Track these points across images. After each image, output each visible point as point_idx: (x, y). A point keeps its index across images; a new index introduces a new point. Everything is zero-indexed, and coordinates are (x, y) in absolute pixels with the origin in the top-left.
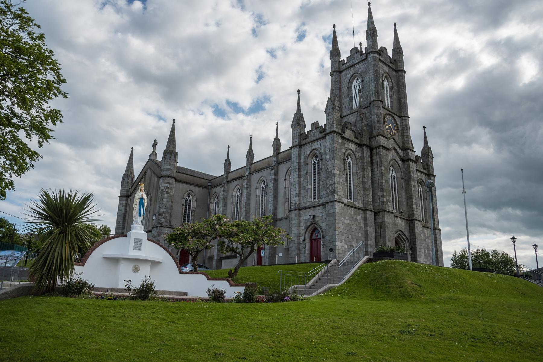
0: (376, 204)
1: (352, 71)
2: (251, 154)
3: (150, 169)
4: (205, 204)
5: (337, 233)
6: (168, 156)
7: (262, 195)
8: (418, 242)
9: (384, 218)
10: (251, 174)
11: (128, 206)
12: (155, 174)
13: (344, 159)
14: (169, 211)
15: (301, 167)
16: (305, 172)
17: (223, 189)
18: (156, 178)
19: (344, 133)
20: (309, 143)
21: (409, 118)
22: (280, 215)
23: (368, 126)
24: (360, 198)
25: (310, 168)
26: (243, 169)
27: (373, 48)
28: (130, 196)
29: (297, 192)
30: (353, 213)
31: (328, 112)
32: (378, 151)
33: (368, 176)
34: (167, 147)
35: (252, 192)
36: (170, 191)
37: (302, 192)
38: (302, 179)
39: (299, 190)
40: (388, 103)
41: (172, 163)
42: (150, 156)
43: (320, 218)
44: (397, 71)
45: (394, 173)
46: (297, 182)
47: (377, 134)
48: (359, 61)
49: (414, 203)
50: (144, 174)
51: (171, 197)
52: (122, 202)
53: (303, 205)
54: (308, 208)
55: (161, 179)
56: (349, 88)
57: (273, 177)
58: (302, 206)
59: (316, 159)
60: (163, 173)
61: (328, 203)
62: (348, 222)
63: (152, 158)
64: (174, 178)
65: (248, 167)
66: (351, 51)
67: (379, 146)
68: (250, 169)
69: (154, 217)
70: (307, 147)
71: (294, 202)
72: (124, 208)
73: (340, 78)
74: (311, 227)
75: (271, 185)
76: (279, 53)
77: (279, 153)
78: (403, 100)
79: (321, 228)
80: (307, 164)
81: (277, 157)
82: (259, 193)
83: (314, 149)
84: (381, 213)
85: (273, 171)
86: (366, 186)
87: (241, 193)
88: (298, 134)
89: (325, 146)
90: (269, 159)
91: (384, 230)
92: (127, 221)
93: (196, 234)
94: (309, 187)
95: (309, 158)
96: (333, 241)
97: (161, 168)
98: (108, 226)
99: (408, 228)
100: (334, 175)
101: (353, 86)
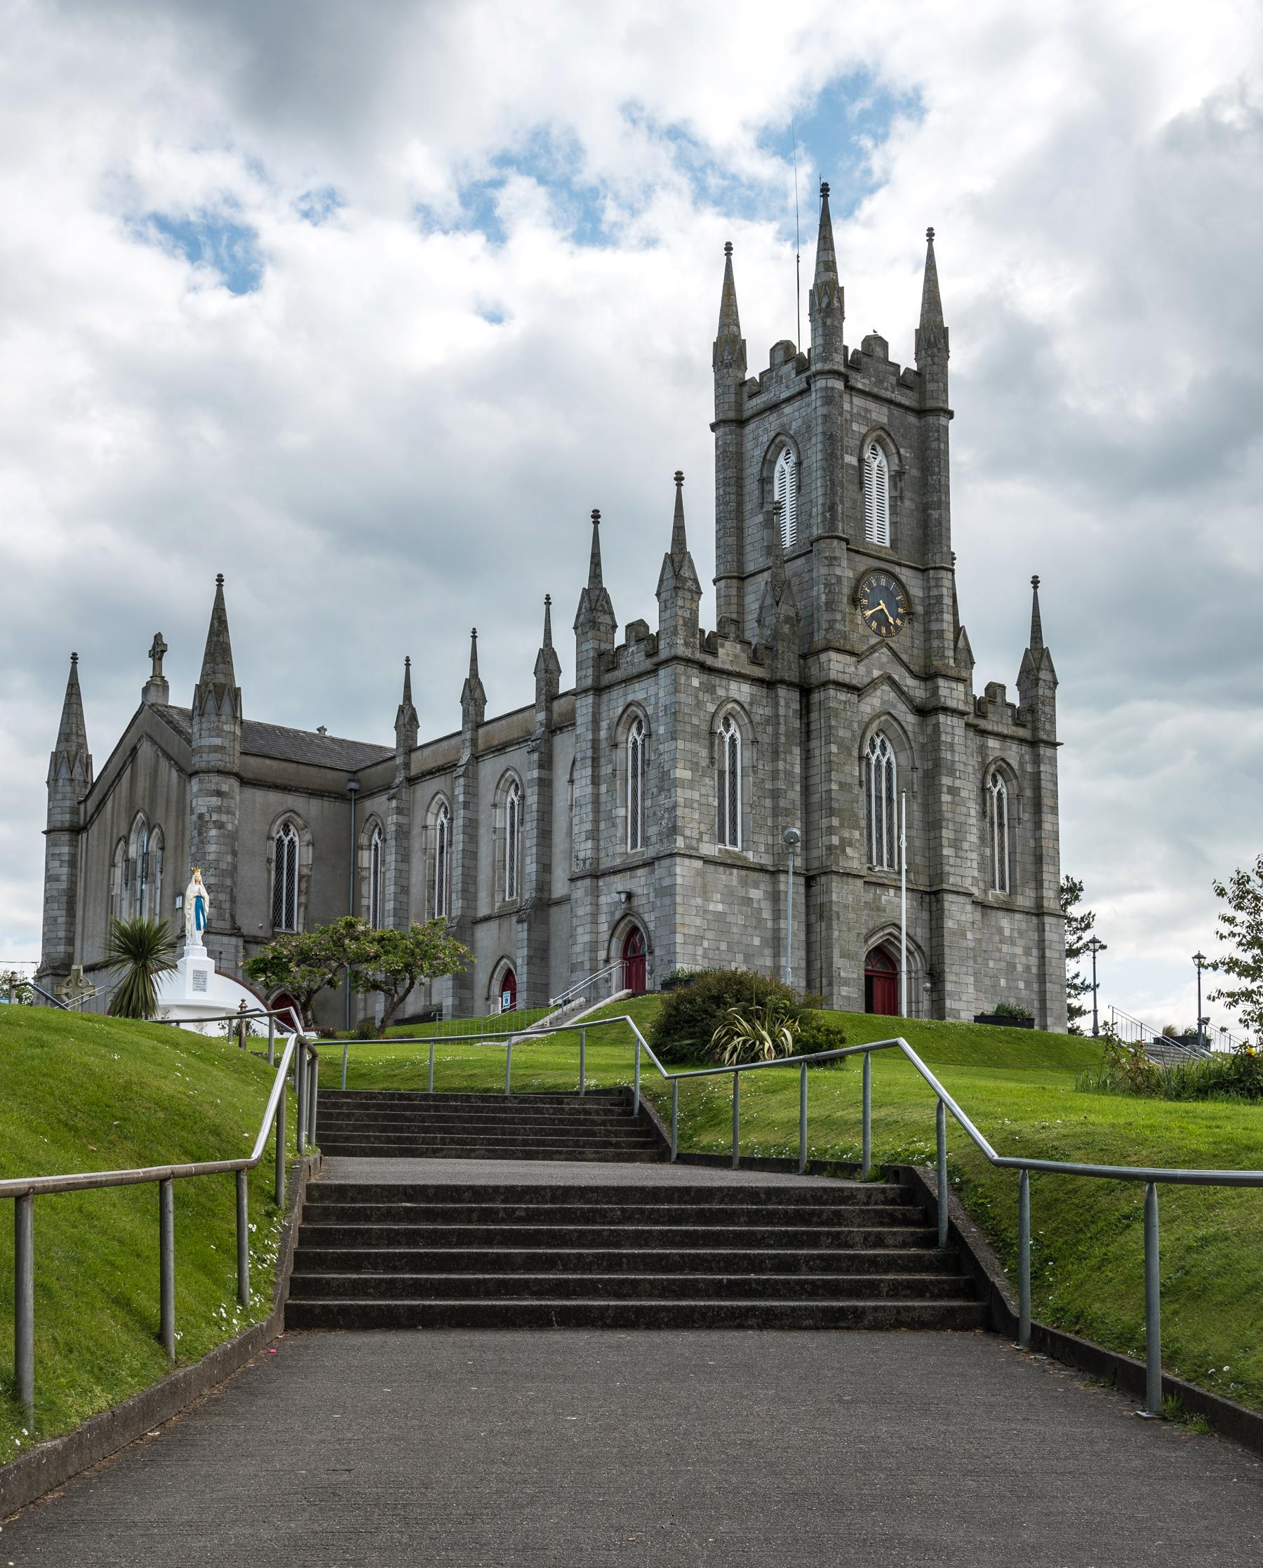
0: (815, 853)
1: (772, 422)
4: (341, 855)
5: (679, 939)
6: (211, 704)
8: (950, 956)
9: (829, 892)
10: (476, 758)
11: (81, 864)
12: (169, 757)
13: (712, 733)
14: (228, 882)
15: (602, 753)
17: (394, 803)
18: (174, 774)
19: (714, 654)
20: (620, 683)
22: (559, 888)
23: (794, 621)
24: (763, 839)
25: (623, 756)
26: (453, 741)
28: (84, 828)
29: (588, 826)
30: (735, 882)
31: (663, 595)
33: (789, 774)
34: (204, 675)
35: (482, 817)
36: (224, 818)
37: (602, 826)
38: (603, 788)
39: (596, 822)
40: (879, 532)
42: (145, 691)
43: (644, 901)
44: (921, 412)
45: (890, 751)
46: (589, 799)
49: (945, 842)
50: (127, 753)
51: (231, 840)
53: (606, 864)
54: (615, 872)
55: (195, 781)
56: (766, 482)
58: (602, 867)
60: (199, 762)
62: (720, 908)
63: (152, 698)
64: (236, 775)
65: (468, 735)
66: (773, 350)
67: (825, 684)
68: (474, 742)
70: (616, 693)
71: (582, 855)
72: (65, 870)
73: (740, 444)
74: (622, 924)
75: (532, 800)
78: (935, 514)
79: (646, 928)
80: (615, 746)
81: (549, 710)
82: (501, 819)
83: (630, 705)
84: (823, 879)
85: (535, 756)
86: (782, 803)
87: (451, 819)
88: (591, 654)
90: (526, 714)
91: (829, 927)
92: (79, 914)
93: (304, 957)
94: (621, 812)
95: (620, 729)
96: (670, 962)
97: (189, 742)
99: (925, 915)
100: (675, 783)
101: (777, 475)
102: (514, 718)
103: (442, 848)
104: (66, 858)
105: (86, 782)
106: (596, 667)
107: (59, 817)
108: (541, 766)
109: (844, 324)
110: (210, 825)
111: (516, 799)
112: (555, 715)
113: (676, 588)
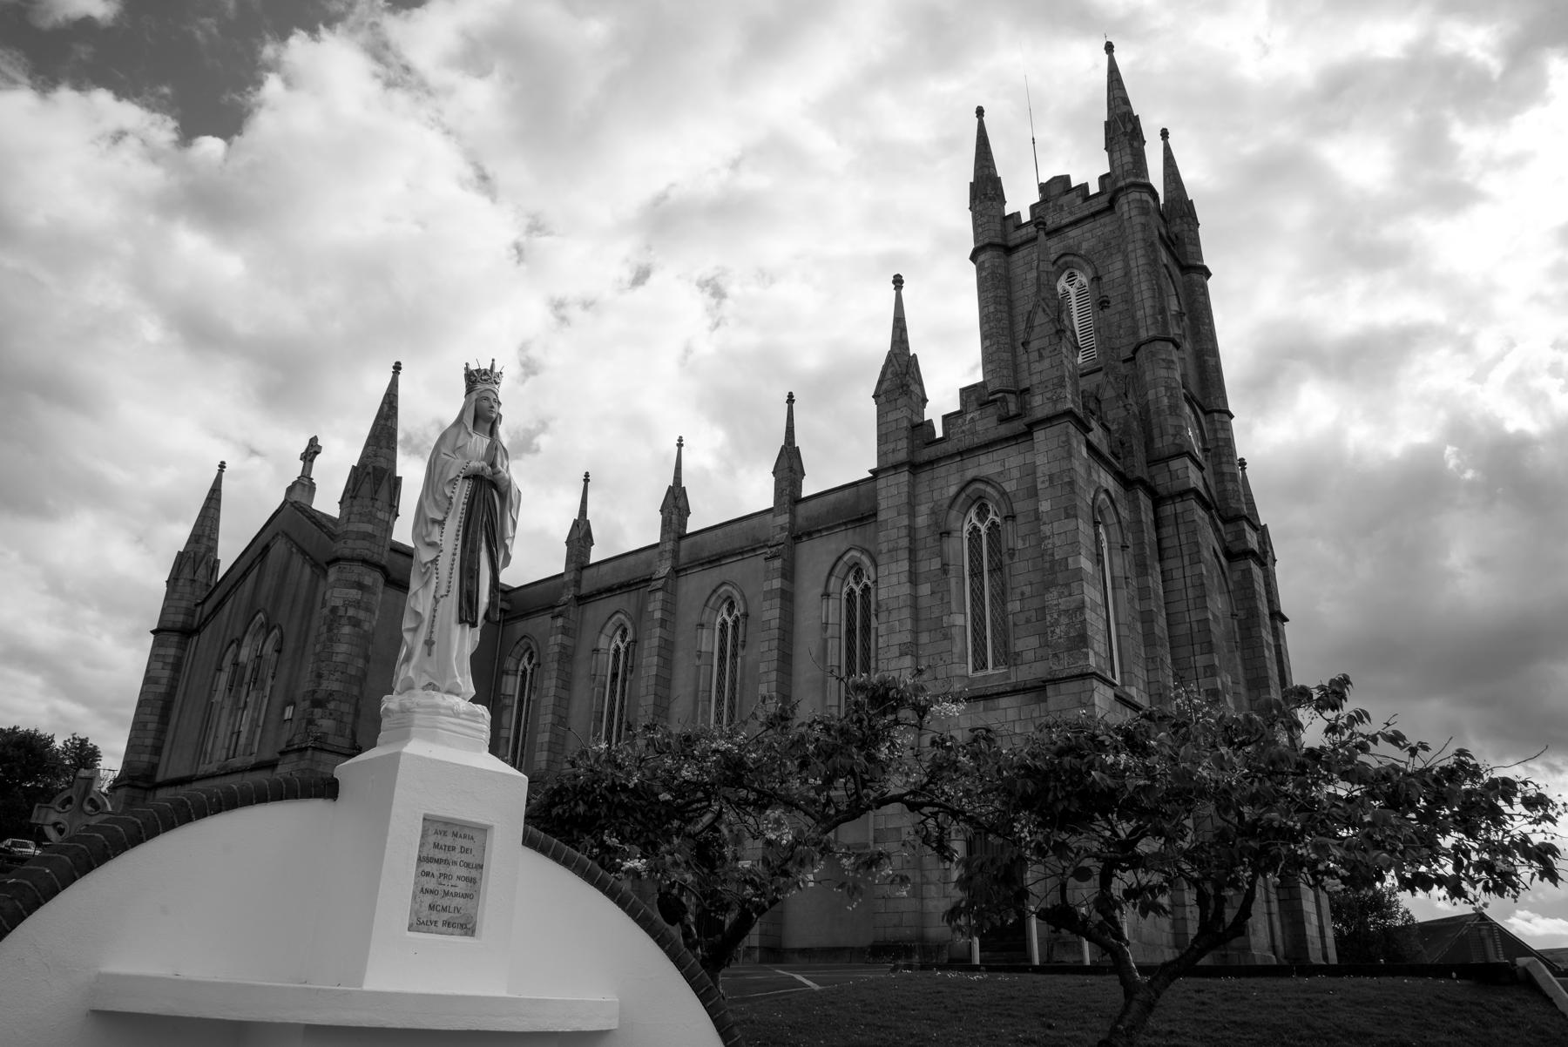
2: (681, 505)
3: (286, 535)
6: (366, 488)
7: (722, 650)
10: (677, 571)
12: (303, 552)
16: (936, 564)
17: (560, 622)
18: (308, 570)
20: (951, 456)
21: (1231, 416)
25: (960, 548)
27: (1137, 176)
28: (197, 631)
29: (906, 637)
32: (1179, 507)
33: (1157, 594)
36: (362, 615)
37: (924, 638)
38: (925, 589)
39: (915, 632)
41: (380, 515)
42: (290, 490)
47: (1173, 450)
48: (1079, 215)
50: (258, 551)
52: (162, 651)
57: (777, 583)
59: (982, 515)
60: (341, 548)
61: (1056, 681)
63: (295, 497)
64: (383, 569)
65: (669, 546)
68: (675, 554)
69: (289, 713)
70: (941, 471)
72: (167, 673)
73: (1007, 270)
75: (771, 613)
76: (575, 312)
77: (797, 500)
78: (1211, 361)
80: (948, 533)
81: (793, 514)
82: (709, 642)
88: (905, 424)
89: (1031, 470)
92: (173, 721)
94: (959, 620)
95: (953, 513)
98: (92, 742)
102: (744, 523)
103: (615, 675)
104: (170, 660)
105: (208, 585)
106: (911, 440)
107: (172, 617)
108: (784, 576)
109: (1146, 147)
110: (344, 621)
111: (730, 621)
112: (800, 520)
113: (1057, 332)
